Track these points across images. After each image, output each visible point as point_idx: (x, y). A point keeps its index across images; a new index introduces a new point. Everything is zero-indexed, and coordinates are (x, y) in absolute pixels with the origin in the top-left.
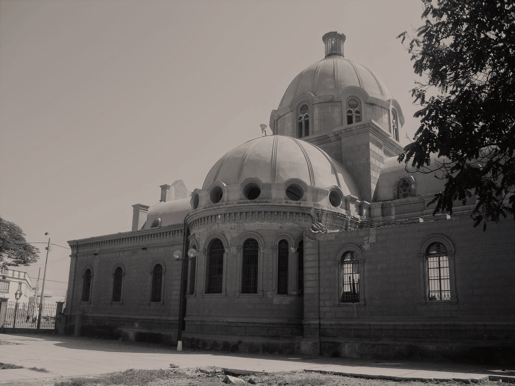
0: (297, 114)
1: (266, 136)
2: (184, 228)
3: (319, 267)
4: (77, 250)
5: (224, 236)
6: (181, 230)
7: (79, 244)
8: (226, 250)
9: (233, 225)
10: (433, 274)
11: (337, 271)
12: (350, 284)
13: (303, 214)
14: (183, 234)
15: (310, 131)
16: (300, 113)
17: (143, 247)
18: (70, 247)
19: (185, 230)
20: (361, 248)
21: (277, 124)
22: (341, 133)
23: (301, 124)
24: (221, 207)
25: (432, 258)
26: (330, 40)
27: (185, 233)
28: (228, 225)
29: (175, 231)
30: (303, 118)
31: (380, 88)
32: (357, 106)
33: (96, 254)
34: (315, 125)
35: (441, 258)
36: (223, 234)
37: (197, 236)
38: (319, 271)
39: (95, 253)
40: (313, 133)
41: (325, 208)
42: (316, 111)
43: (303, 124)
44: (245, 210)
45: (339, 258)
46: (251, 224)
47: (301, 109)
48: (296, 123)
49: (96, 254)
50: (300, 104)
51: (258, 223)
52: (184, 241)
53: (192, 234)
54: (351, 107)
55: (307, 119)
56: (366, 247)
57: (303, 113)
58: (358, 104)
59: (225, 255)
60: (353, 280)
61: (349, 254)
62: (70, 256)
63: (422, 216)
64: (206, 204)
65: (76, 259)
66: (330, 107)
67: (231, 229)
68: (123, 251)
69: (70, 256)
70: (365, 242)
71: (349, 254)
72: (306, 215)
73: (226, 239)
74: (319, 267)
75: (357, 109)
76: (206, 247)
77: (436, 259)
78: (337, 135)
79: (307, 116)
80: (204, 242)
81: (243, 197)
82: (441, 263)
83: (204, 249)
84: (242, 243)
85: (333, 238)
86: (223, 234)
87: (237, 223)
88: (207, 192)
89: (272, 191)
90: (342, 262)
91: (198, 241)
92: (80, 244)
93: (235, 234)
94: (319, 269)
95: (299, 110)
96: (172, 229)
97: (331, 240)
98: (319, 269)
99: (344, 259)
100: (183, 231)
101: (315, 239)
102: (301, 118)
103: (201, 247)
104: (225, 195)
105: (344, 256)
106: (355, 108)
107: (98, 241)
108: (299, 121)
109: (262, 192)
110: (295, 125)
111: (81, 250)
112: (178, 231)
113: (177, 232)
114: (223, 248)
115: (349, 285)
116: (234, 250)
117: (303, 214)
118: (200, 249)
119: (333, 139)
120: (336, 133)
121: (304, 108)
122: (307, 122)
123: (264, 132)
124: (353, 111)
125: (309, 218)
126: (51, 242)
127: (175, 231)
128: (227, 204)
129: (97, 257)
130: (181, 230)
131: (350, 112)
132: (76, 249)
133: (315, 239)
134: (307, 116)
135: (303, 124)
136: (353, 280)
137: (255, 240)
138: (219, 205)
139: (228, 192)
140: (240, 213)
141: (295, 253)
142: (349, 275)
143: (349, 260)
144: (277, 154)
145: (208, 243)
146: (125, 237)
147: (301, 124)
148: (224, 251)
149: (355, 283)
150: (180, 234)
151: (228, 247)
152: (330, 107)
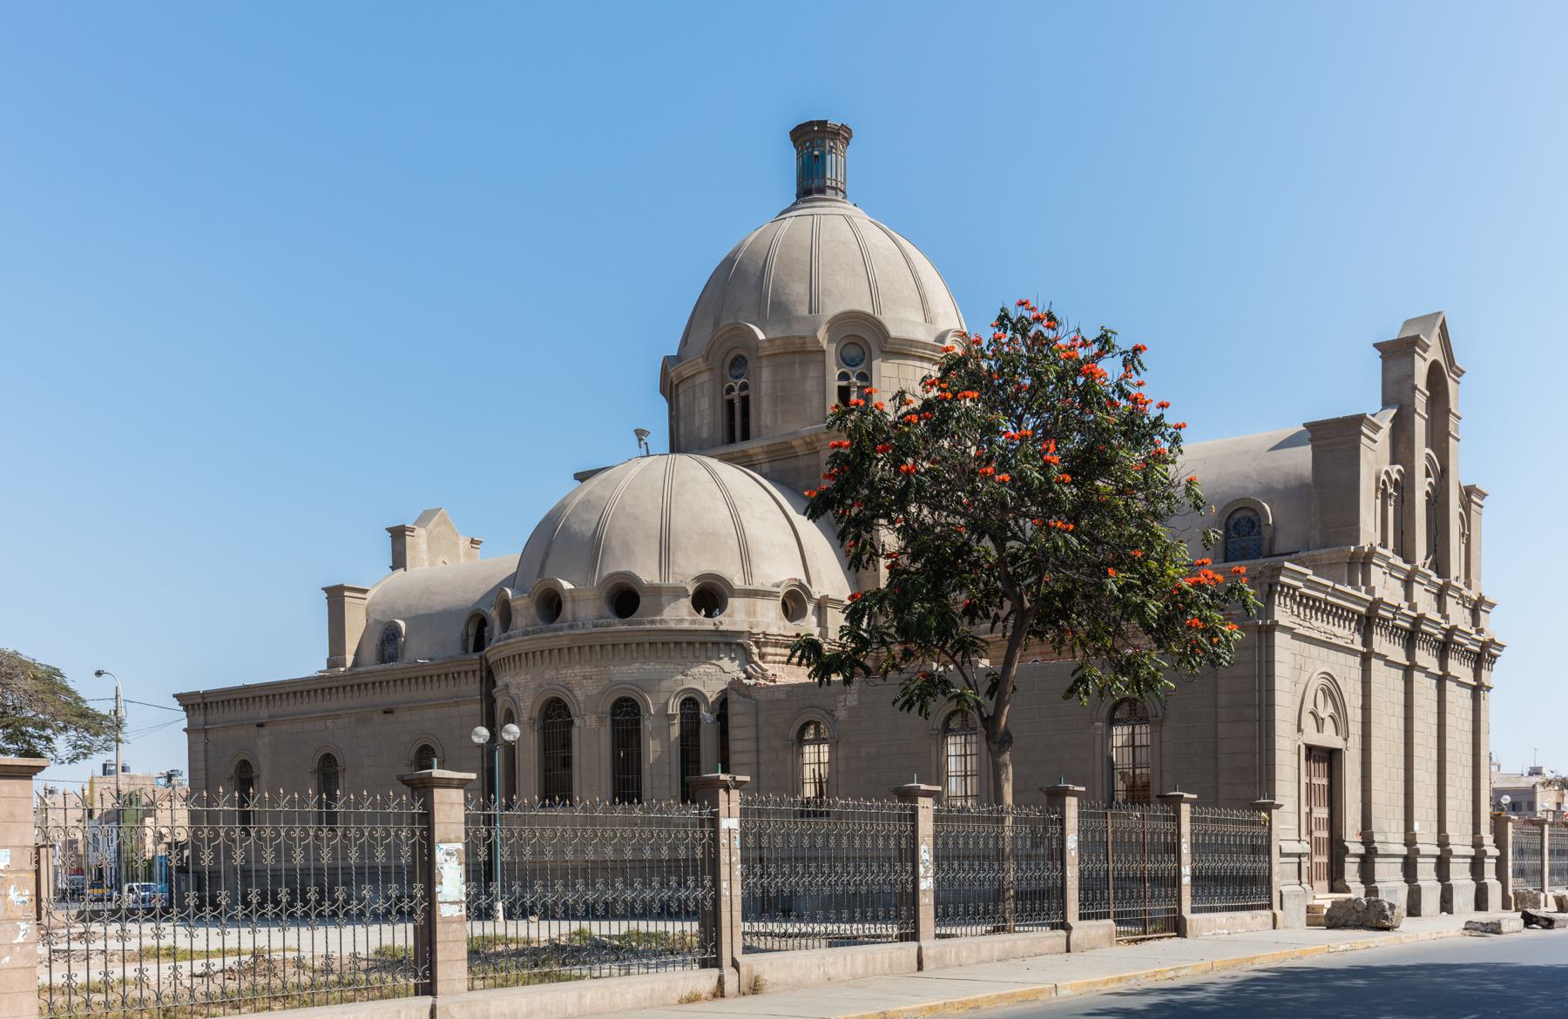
0: (723, 379)
1: (648, 455)
2: (478, 666)
3: (758, 751)
4: (205, 715)
5: (571, 692)
6: (474, 672)
7: (207, 700)
8: (577, 721)
9: (588, 670)
10: (827, 755)
11: (789, 760)
12: (815, 783)
13: (728, 644)
14: (478, 679)
15: (753, 429)
16: (729, 378)
17: (384, 708)
18: (182, 708)
19: (481, 671)
20: (833, 716)
21: (677, 395)
22: (819, 440)
23: (731, 403)
24: (561, 633)
25: (1119, 728)
26: (808, 144)
27: (481, 678)
28: (577, 670)
29: (459, 673)
30: (737, 388)
31: (923, 301)
32: (862, 360)
33: (260, 725)
34: (764, 414)
35: (1137, 728)
36: (568, 689)
37: (513, 691)
38: (758, 760)
39: (256, 722)
40: (759, 435)
41: (773, 630)
42: (766, 375)
43: (738, 405)
44: (609, 640)
45: (793, 734)
46: (624, 669)
47: (732, 365)
48: (719, 400)
49: (260, 725)
50: (729, 351)
51: (637, 665)
52: (481, 695)
53: (500, 683)
54: (848, 365)
55: (744, 393)
56: (841, 714)
57: (737, 377)
58: (864, 354)
59: (575, 731)
60: (820, 775)
61: (812, 727)
62: (185, 730)
63: (1324, 554)
64: (527, 625)
65: (206, 738)
66: (797, 365)
67: (585, 678)
68: (337, 717)
69: (185, 730)
70: (840, 705)
71: (812, 727)
72: (734, 646)
73: (576, 698)
74: (758, 751)
75: (859, 369)
76: (536, 714)
77: (1126, 730)
78: (811, 443)
79: (744, 387)
80: (529, 703)
81: (607, 611)
82: (1137, 738)
83: (530, 719)
84: (607, 707)
85: (783, 696)
86: (568, 689)
87: (596, 667)
88: (528, 600)
89: (663, 599)
90: (801, 741)
91: (517, 701)
92: (211, 699)
93: (592, 688)
94: (758, 755)
95: (726, 370)
96: (452, 669)
97: (780, 700)
98: (758, 755)
99: (803, 735)
100: (478, 673)
101: (750, 697)
102: (730, 389)
103: (525, 715)
104: (567, 607)
105: (803, 729)
106: (857, 365)
107: (262, 693)
108: (728, 397)
109: (644, 601)
110: (719, 407)
111: (214, 716)
112: (466, 672)
113: (463, 675)
114: (569, 715)
115: (813, 785)
116: (591, 721)
117: (728, 644)
118: (522, 719)
119: (801, 450)
120: (808, 440)
121: (739, 363)
122: (745, 401)
123: (644, 446)
124: (850, 373)
125: (740, 652)
126: (122, 696)
127: (459, 673)
128: (571, 627)
129: (264, 731)
130: (474, 672)
131: (844, 376)
132: (202, 712)
133: (750, 697)
134: (744, 387)
135: (738, 405)
136: (820, 775)
137: (633, 700)
138: (556, 630)
139: (573, 601)
140: (601, 646)
141: (713, 723)
142: (812, 766)
143: (811, 737)
144: (672, 515)
145: (538, 707)
146: (335, 684)
147: (731, 403)
148: (572, 722)
149: (824, 780)
150: (471, 679)
151: (582, 717)
152: (797, 365)
